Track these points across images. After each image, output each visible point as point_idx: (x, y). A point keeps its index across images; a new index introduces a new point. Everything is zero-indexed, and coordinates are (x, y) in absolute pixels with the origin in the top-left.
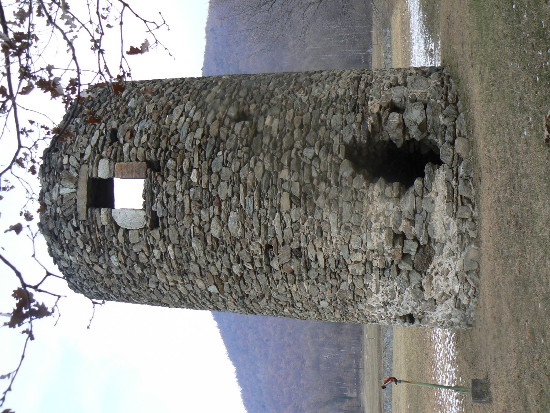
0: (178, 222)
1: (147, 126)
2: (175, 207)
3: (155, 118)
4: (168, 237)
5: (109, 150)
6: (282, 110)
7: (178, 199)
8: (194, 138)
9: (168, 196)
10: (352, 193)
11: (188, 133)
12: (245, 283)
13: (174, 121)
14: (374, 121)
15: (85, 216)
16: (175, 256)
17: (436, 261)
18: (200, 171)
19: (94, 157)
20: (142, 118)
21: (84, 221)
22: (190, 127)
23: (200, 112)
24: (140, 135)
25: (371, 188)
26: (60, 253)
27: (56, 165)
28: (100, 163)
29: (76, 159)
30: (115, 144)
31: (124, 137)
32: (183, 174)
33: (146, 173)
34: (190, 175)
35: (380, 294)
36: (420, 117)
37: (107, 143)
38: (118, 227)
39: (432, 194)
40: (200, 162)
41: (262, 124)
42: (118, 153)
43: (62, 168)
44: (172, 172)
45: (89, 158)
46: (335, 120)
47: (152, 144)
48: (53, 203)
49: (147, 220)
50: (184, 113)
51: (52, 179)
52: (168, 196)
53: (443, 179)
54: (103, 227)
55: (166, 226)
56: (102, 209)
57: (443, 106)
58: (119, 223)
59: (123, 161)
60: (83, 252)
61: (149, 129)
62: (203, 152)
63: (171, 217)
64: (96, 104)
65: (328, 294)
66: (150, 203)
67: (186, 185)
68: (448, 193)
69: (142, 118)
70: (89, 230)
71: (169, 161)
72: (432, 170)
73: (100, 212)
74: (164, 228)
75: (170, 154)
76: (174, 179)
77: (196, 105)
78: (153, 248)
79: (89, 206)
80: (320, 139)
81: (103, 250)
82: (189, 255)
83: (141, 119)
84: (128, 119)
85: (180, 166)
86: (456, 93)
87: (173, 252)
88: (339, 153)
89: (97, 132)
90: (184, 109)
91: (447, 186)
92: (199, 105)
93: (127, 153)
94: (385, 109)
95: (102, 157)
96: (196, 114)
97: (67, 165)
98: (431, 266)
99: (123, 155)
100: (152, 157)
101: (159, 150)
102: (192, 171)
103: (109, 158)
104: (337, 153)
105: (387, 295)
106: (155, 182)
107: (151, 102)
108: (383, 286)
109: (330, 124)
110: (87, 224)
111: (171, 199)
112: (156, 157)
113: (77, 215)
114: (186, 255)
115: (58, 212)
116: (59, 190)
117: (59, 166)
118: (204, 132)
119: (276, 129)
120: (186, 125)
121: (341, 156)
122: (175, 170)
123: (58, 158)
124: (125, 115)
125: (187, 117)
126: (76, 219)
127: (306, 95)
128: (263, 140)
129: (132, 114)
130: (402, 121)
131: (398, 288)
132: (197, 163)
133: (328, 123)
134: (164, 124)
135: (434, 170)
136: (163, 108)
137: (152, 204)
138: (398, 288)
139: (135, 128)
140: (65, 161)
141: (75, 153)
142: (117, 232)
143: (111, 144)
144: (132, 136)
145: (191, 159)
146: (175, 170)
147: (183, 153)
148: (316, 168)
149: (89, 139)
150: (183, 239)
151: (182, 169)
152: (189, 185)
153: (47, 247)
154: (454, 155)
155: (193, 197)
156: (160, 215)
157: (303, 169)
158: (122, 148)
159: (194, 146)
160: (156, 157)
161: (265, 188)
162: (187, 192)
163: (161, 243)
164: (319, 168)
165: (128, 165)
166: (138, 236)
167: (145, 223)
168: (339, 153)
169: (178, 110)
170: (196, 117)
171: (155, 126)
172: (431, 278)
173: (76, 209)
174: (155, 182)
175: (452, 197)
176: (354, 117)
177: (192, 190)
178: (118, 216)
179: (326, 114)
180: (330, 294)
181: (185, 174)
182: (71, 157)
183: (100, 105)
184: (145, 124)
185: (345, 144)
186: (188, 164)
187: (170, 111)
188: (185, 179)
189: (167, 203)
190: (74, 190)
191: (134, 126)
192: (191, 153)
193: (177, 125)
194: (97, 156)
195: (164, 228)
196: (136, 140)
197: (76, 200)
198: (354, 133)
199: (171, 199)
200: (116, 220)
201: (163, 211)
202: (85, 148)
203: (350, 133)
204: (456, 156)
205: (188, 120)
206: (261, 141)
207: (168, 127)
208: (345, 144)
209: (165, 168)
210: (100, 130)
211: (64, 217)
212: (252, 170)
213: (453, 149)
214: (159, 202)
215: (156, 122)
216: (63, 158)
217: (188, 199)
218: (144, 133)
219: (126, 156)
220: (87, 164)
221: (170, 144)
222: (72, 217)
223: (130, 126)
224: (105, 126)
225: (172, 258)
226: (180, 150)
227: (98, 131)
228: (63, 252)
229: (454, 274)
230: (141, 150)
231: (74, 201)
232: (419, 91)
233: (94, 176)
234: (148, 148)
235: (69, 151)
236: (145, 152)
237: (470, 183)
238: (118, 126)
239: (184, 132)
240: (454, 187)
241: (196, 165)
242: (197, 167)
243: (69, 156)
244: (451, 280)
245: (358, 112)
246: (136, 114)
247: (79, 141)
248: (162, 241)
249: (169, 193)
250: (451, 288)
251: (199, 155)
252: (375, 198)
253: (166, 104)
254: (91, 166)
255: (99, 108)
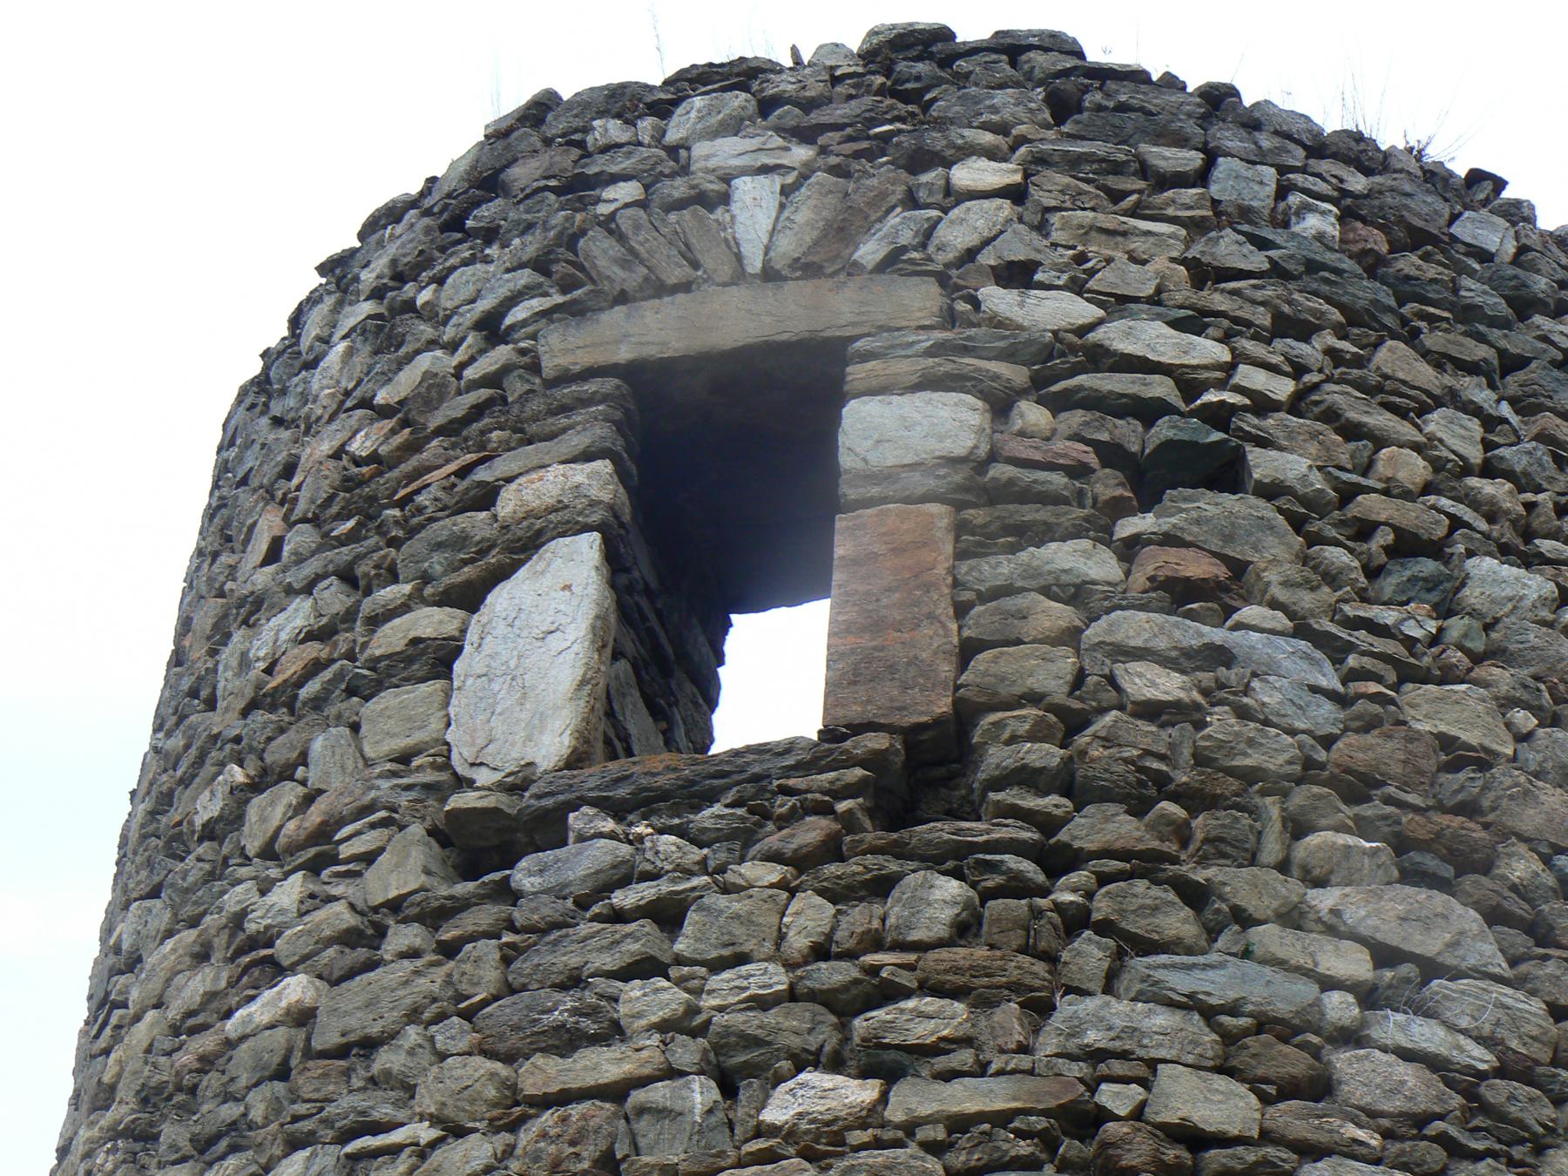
0: (468, 1015)
1: (1267, 695)
2: (574, 981)
3: (1356, 750)
4: (371, 966)
5: (1060, 445)
7: (634, 990)
8: (1153, 1064)
9: (668, 914)
11: (1209, 1013)
13: (1324, 900)
15: (563, 361)
16: (243, 1038)
18: (857, 1137)
19: (1008, 355)
20: (1352, 661)
21: (535, 367)
22: (1263, 1023)
23: (1422, 1105)
24: (1188, 653)
26: (368, 277)
27: (941, 124)
28: (954, 396)
29: (987, 242)
30: (1108, 485)
31: (1169, 540)
32: (843, 1005)
33: (858, 729)
34: (836, 1065)
37: (1128, 433)
38: (469, 598)
40: (939, 1133)
42: (1032, 513)
43: (919, 161)
44: (860, 917)
45: (997, 322)
47: (1108, 741)
48: (673, 151)
49: (501, 787)
50: (1403, 977)
51: (840, 112)
52: (668, 914)
54: (486, 498)
55: (448, 934)
56: (604, 466)
58: (500, 599)
59: (961, 555)
60: (359, 412)
61: (1243, 714)
62: (1024, 1148)
63: (507, 961)
64: (1481, 338)
66: (622, 792)
67: (754, 1042)
69: (1352, 661)
70: (478, 411)
71: (949, 889)
73: (587, 456)
74: (434, 917)
75: (1018, 888)
76: (798, 942)
77: (1501, 1072)
78: (314, 868)
79: (635, 374)
81: (352, 537)
82: (234, 1149)
83: (1336, 650)
84: (1336, 556)
85: (907, 979)
87: (266, 1019)
89: (1207, 350)
90: (1456, 974)
92: (1497, 1091)
93: (1031, 572)
95: (1000, 405)
96: (1408, 1074)
97: (948, 190)
99: (1013, 549)
100: (997, 758)
101: (1052, 803)
102: (864, 1074)
103: (993, 457)
106: (783, 805)
107: (1523, 719)
110: (516, 387)
111: (641, 939)
112: (998, 784)
113: (575, 311)
114: (233, 1126)
115: (609, 193)
116: (765, 170)
117: (935, 140)
118: (1223, 1141)
120: (1288, 996)
122: (875, 942)
123: (1002, 129)
124: (1384, 537)
125: (1369, 997)
126: (546, 314)
129: (1389, 585)
132: (925, 1110)
134: (1298, 828)
136: (1469, 809)
137: (618, 810)
139: (1250, 613)
140: (968, 174)
141: (1042, 228)
142: (445, 599)
143: (1111, 454)
144: (1179, 594)
145: (964, 1058)
146: (875, 942)
147: (1015, 987)
149: (1155, 300)
150: (347, 1073)
151: (889, 993)
152: (750, 1070)
153: (415, 188)
155: (642, 1111)
156: (525, 875)
158: (1076, 534)
159: (1078, 1069)
160: (998, 784)
162: (686, 1052)
163: (337, 916)
165: (927, 588)
166: (401, 743)
167: (483, 777)
169: (1447, 924)
170: (1364, 1075)
171: (1276, 753)
173: (622, 298)
174: (783, 805)
177: (700, 1094)
178: (547, 580)
181: (844, 1028)
182: (1005, 207)
183: (1472, 368)
184: (1290, 680)
186: (922, 1032)
187: (1430, 862)
188: (794, 1026)
189: (618, 916)
190: (754, 263)
191: (1274, 605)
192: (1023, 1049)
193: (1293, 918)
194: (1016, 374)
195: (434, 917)
196: (1136, 626)
197: (685, 287)
199: (641, 939)
200: (522, 573)
201: (559, 892)
202: (1077, 287)
205: (1340, 1007)
207: (1272, 849)
209: (893, 866)
210: (1230, 368)
211: (571, 240)
214: (625, 850)
215: (1309, 764)
216: (992, 154)
217: (627, 1068)
218: (1206, 678)
219: (1000, 568)
220: (950, 318)
221: (1103, 879)
222: (564, 290)
223: (1272, 576)
224: (1262, 405)
225: (232, 1027)
226: (1051, 958)
227: (1222, 354)
228: (377, 294)
230: (1051, 673)
231: (676, 272)
233: (857, 373)
234: (1072, 723)
235: (1052, 185)
236: (1034, 698)
238: (1271, 491)
239: (1219, 980)
241: (916, 1099)
242: (895, 1112)
243: (1016, 194)
246: (1388, 616)
247: (1138, 245)
248: (349, 920)
249: (692, 916)
251: (1002, 1119)
253: (1507, 834)
254: (928, 340)
255: (1439, 361)
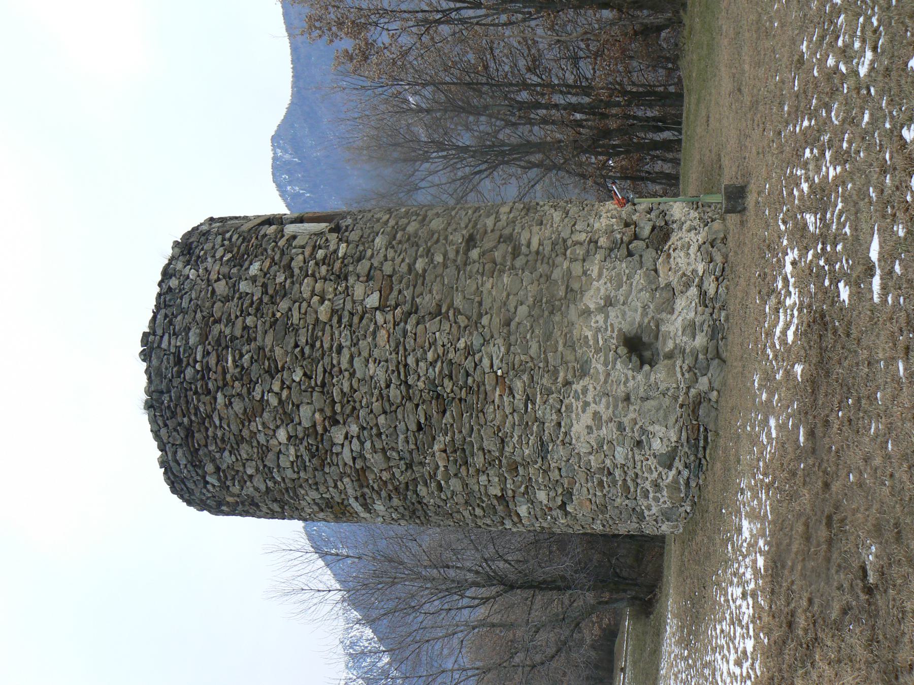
12: (423, 285)
17: (674, 238)
35: (602, 281)
65: (533, 289)
98: (670, 243)
105: (611, 282)
108: (607, 269)
131: (627, 271)
138: (627, 271)
172: (669, 256)
180: (536, 288)
229: (696, 248)
244: (693, 256)
250: (693, 266)
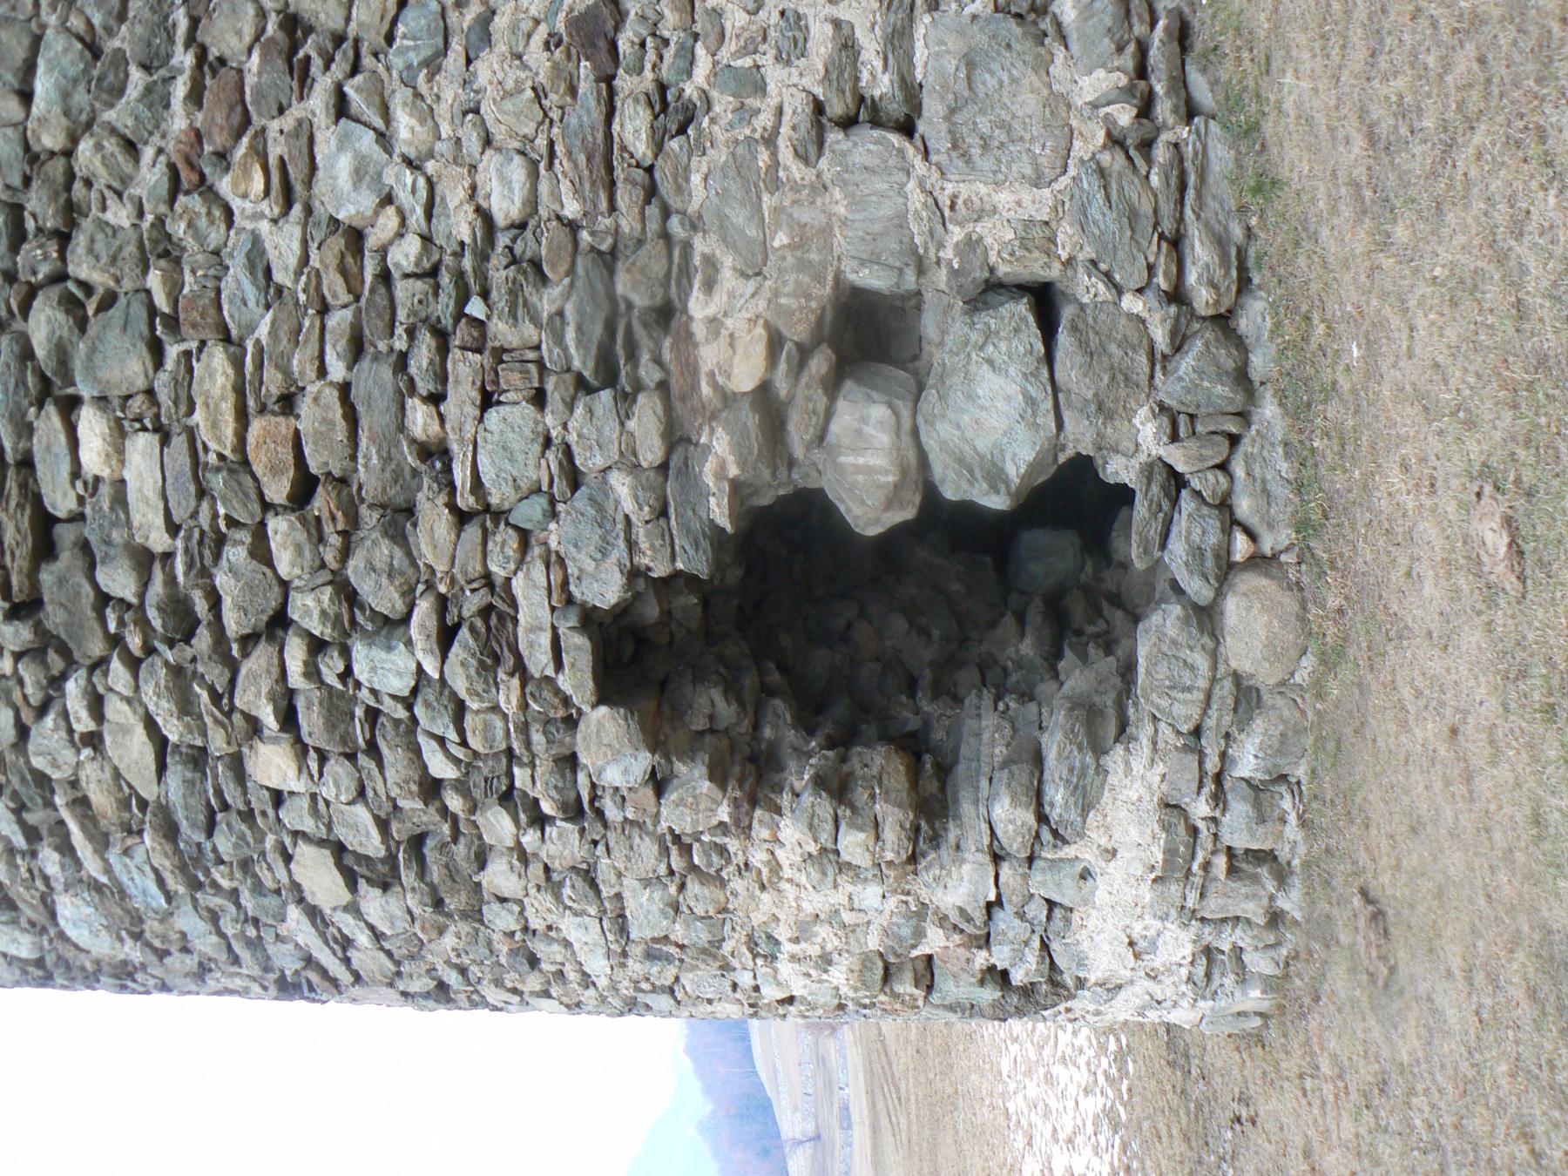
6: (157, 351)
10: (665, 851)
14: (742, 464)
25: (761, 832)
36: (1021, 431)
39: (1083, 852)
41: (65, 469)
46: (501, 449)
53: (1151, 804)
57: (1160, 336)
68: (1170, 852)
72: (1089, 759)
80: (430, 586)
86: (1237, 232)
88: (559, 665)
91: (1166, 827)
94: (804, 353)
104: (550, 672)
109: (477, 484)
119: (159, 520)
121: (577, 681)
127: (288, 204)
128: (101, 577)
130: (911, 456)
133: (461, 475)
135: (1099, 751)
148: (441, 741)
154: (1214, 680)
157: (373, 749)
161: (194, 825)
164: (464, 743)
168: (559, 665)
175: (1184, 855)
176: (611, 430)
179: (436, 399)
185: (590, 619)
198: (631, 545)
203: (604, 554)
204: (1226, 689)
206: (87, 589)
208: (590, 619)
212: (93, 740)
213: (1214, 656)
232: (1004, 198)
237: (1287, 804)
240: (1201, 825)
245: (638, 387)
252: (787, 872)
